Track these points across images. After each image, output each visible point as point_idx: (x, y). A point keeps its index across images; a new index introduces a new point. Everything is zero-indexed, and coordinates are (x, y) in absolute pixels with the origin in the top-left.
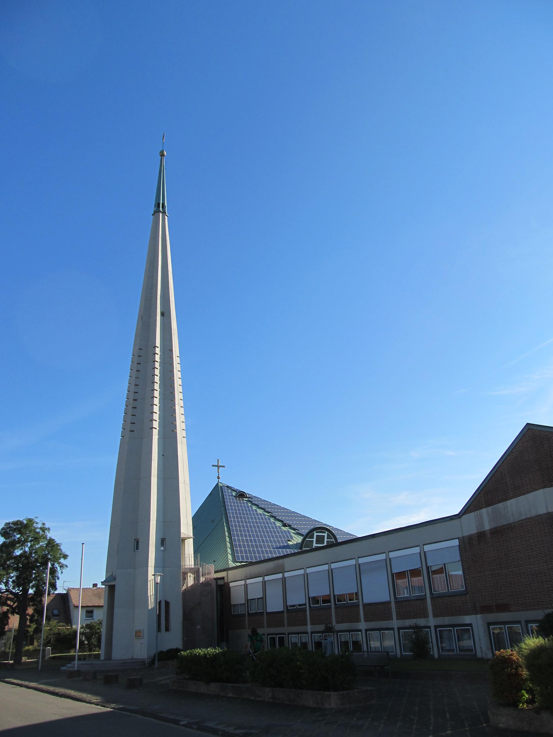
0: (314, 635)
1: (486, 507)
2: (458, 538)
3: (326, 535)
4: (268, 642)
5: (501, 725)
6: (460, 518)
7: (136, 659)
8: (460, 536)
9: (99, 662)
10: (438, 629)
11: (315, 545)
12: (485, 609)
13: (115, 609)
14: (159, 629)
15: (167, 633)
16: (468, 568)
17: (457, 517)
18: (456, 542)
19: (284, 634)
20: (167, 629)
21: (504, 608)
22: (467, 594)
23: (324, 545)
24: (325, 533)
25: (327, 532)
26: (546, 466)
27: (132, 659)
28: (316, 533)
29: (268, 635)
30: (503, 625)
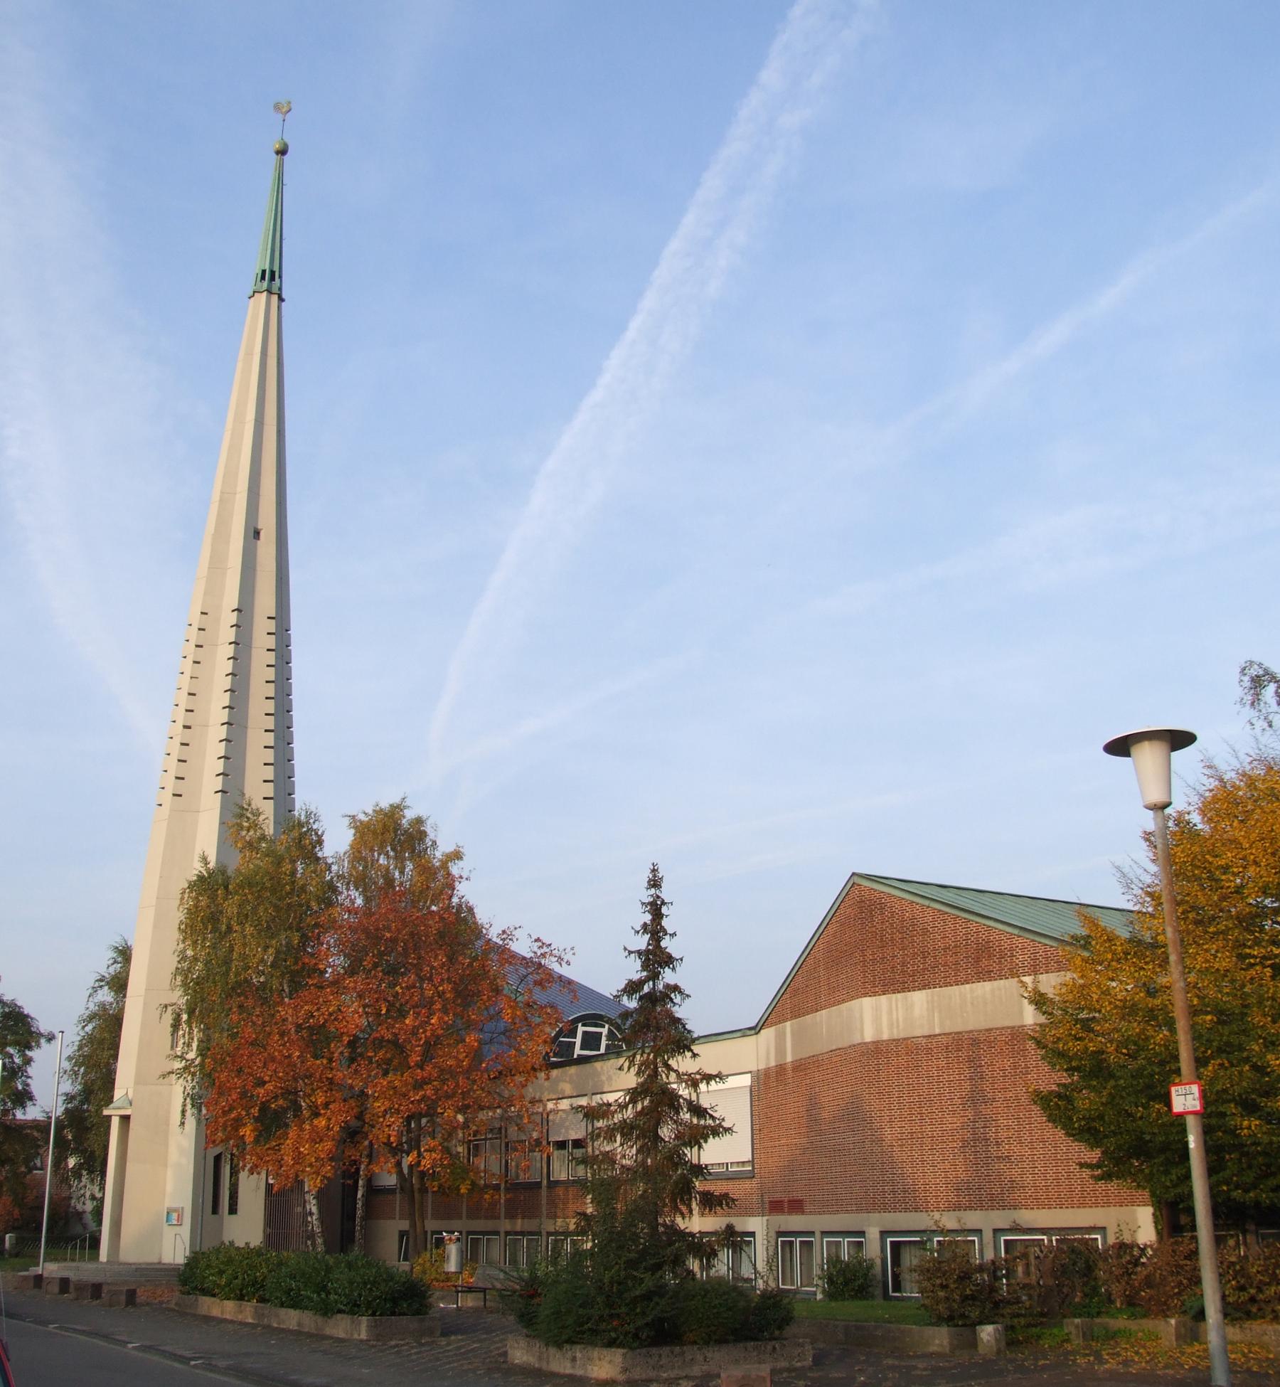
0: (974, 1241)
1: (792, 1018)
2: (751, 1072)
3: (605, 1031)
4: (823, 1254)
5: (517, 1361)
6: (757, 1034)
7: (164, 1264)
8: (754, 1069)
9: (100, 1266)
10: (889, 1240)
11: (578, 1051)
12: (776, 1207)
13: (128, 1164)
14: (215, 1210)
15: (233, 1217)
16: (760, 1130)
17: (753, 1032)
18: (746, 1080)
19: (812, 1233)
20: (233, 1210)
21: (796, 1206)
22: (754, 1177)
23: (598, 1053)
24: (604, 1027)
25: (607, 1026)
26: (871, 958)
27: (160, 1263)
28: (583, 1026)
29: (824, 1233)
30: (1045, 1235)
